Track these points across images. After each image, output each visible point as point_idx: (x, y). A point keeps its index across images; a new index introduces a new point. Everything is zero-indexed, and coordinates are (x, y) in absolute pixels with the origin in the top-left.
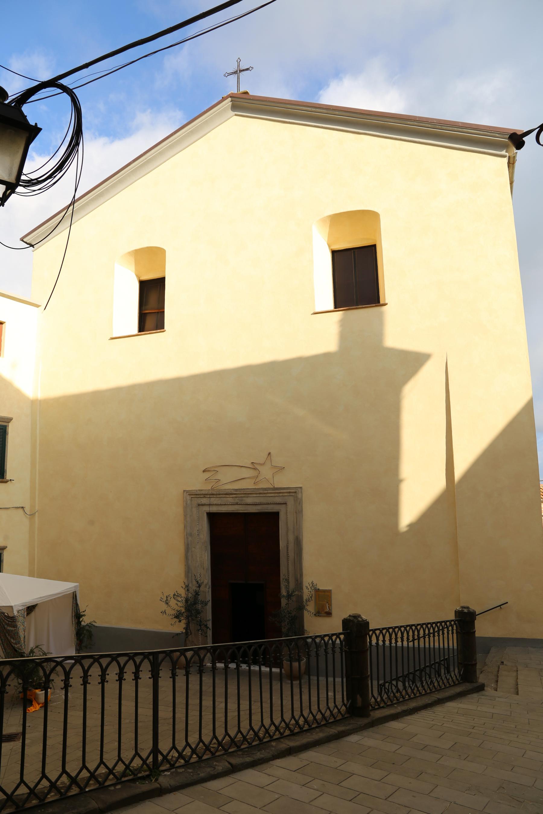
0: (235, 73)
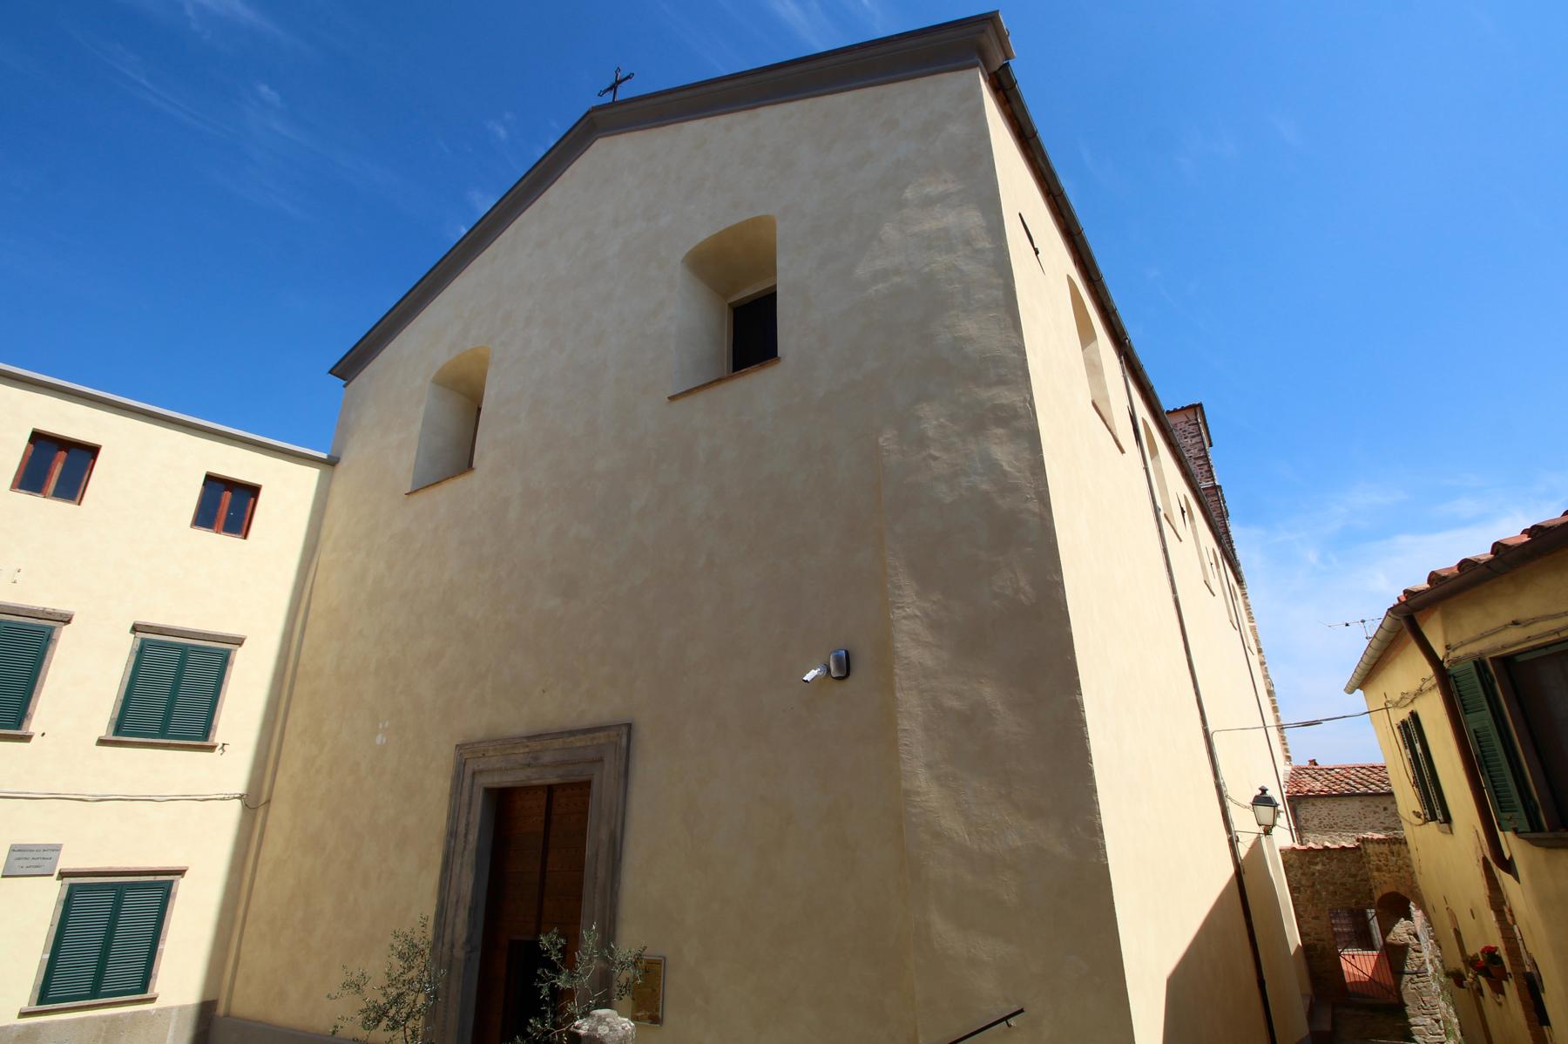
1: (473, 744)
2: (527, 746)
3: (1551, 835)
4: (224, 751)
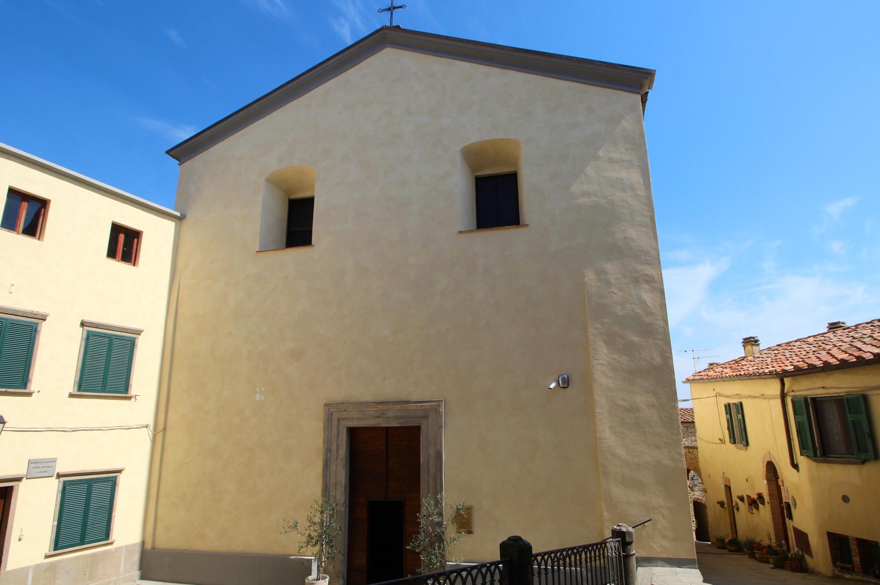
0: (389, 9)
1: (337, 404)
2: (377, 407)
3: (822, 459)
4: (136, 399)
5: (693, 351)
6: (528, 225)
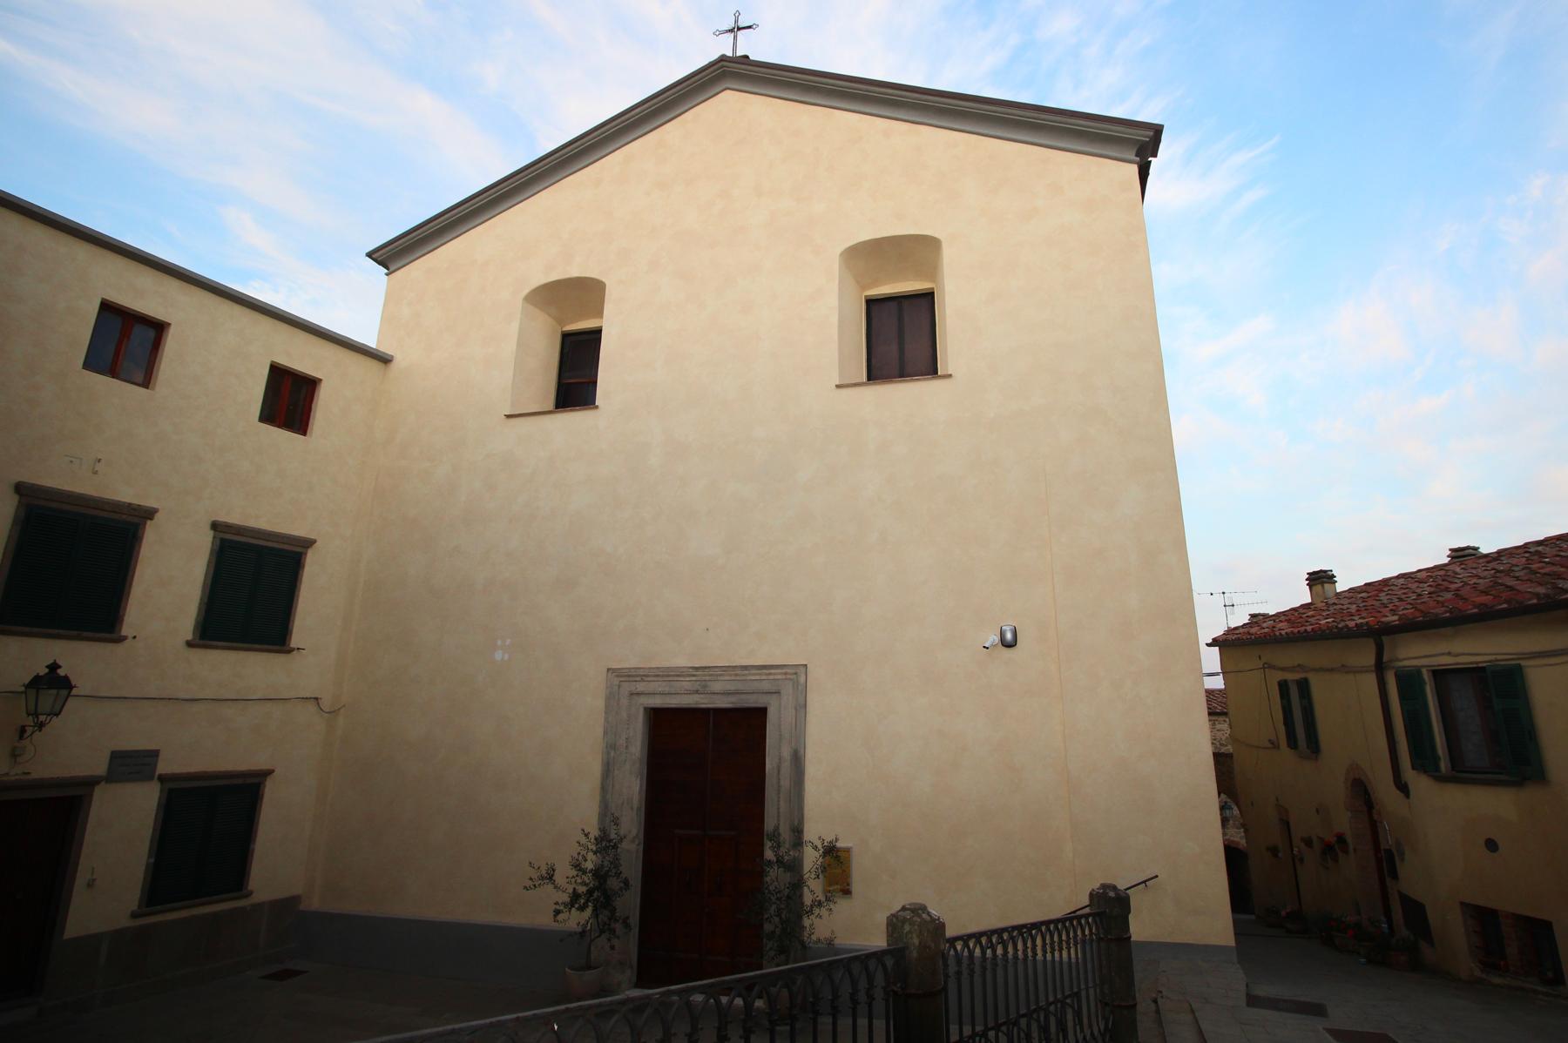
0: (731, 31)
5: (1224, 593)
6: (950, 376)
